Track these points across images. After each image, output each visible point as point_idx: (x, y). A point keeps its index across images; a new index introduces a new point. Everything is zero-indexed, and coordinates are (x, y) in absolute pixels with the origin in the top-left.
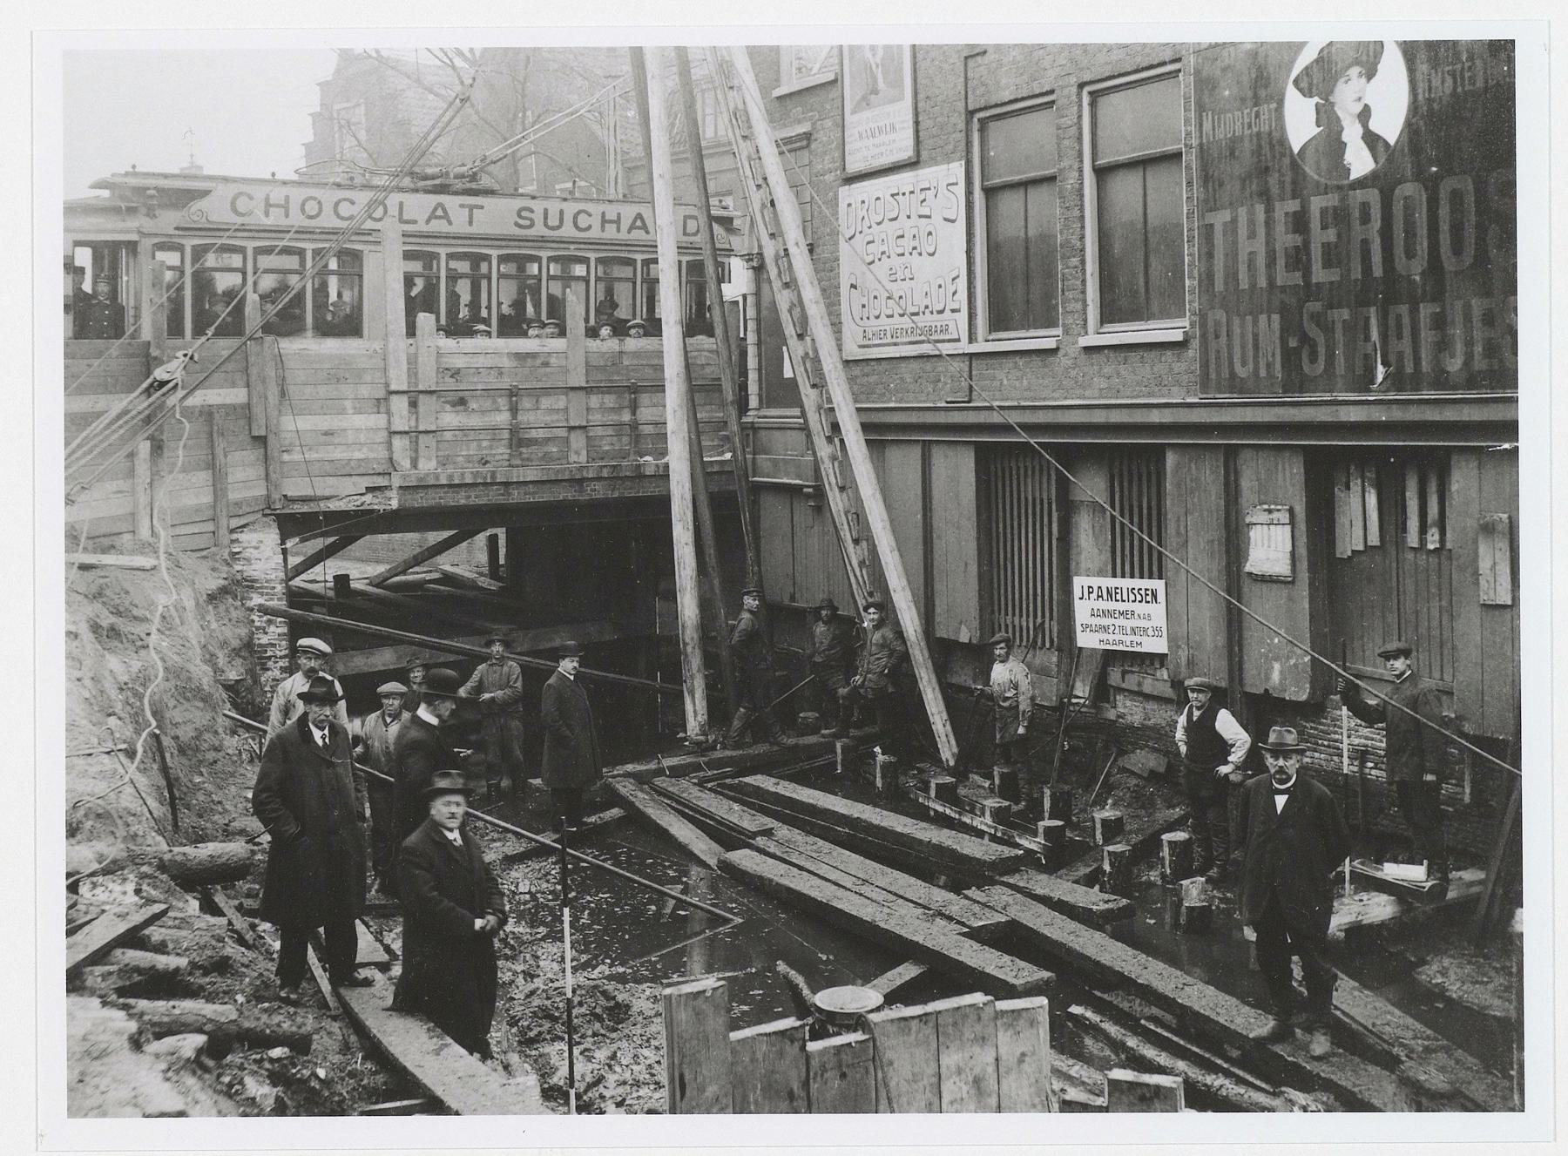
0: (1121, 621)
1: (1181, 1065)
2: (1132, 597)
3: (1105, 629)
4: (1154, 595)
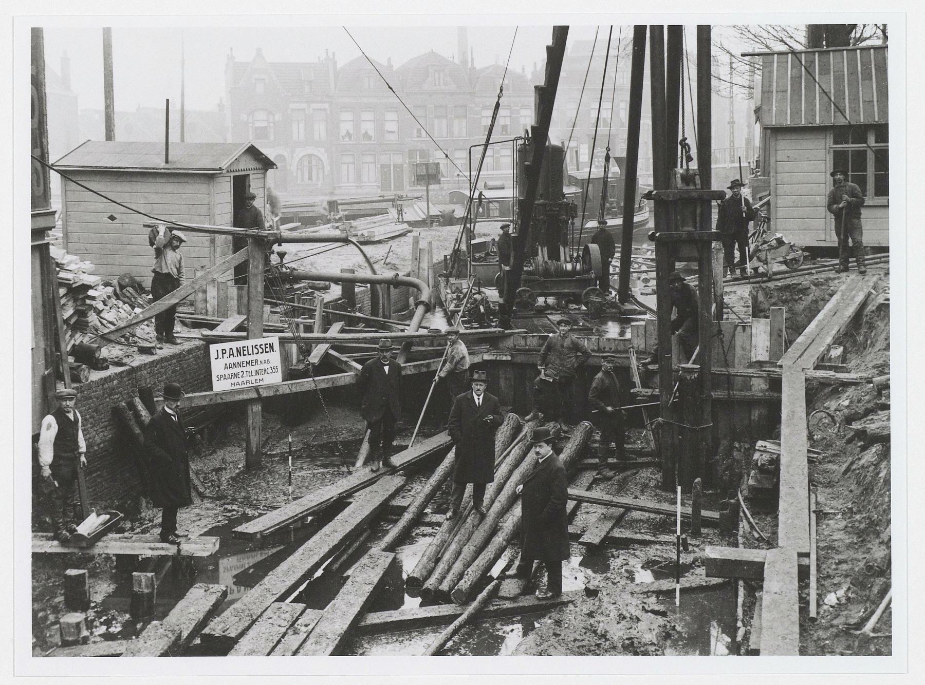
0: (249, 368)
1: (508, 605)
2: (255, 351)
3: (236, 375)
4: (272, 347)
